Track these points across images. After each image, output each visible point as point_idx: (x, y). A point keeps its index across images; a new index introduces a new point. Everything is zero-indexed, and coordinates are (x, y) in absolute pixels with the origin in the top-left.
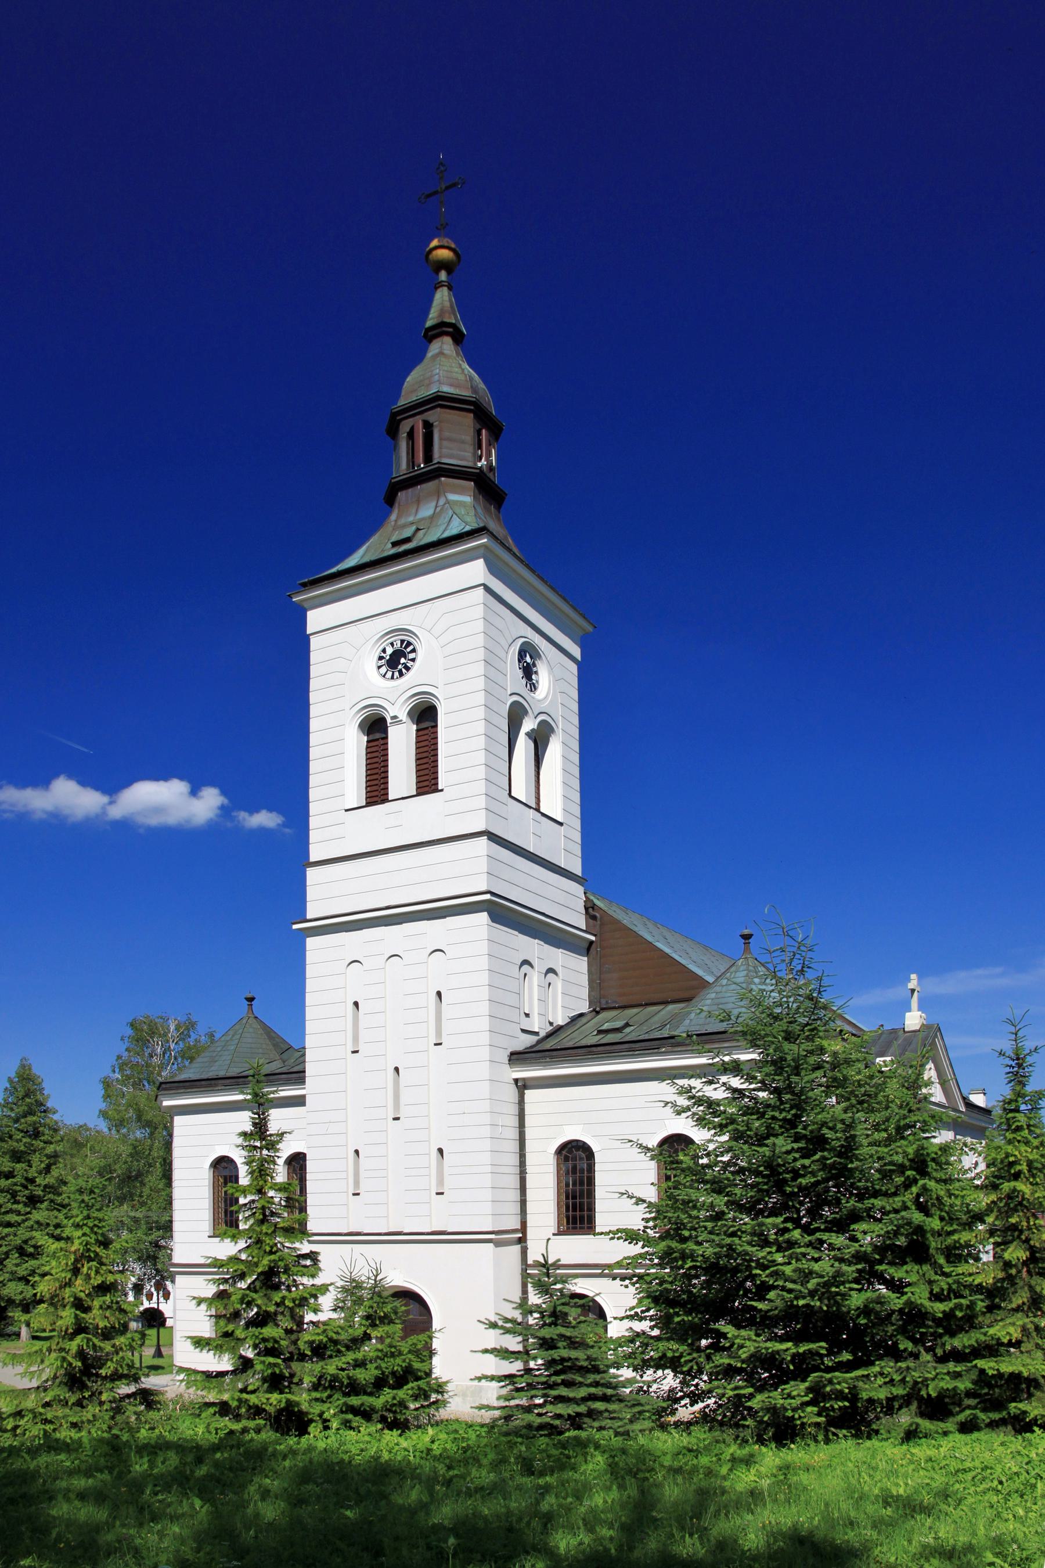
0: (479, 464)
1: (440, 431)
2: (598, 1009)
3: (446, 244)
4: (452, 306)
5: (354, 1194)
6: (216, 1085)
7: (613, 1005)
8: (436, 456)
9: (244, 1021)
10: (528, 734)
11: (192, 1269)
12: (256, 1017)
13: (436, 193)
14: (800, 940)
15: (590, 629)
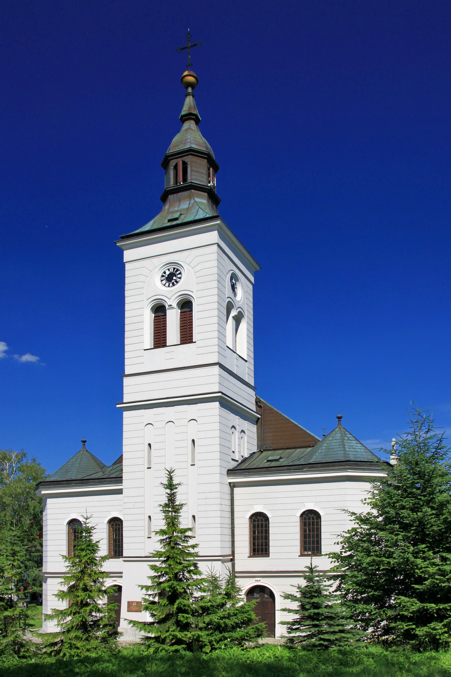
0: (209, 185)
1: (191, 167)
2: (262, 450)
3: (192, 74)
4: (194, 106)
5: (148, 538)
6: (71, 484)
7: (269, 449)
8: (189, 179)
9: (81, 452)
10: (233, 317)
11: (55, 575)
12: (87, 451)
13: (186, 48)
14: (424, 418)
15: (258, 268)
